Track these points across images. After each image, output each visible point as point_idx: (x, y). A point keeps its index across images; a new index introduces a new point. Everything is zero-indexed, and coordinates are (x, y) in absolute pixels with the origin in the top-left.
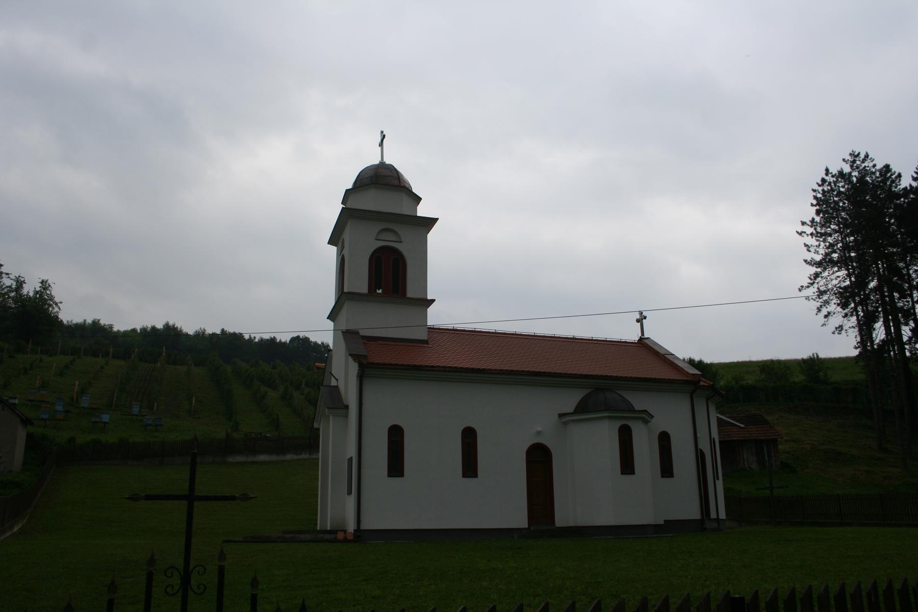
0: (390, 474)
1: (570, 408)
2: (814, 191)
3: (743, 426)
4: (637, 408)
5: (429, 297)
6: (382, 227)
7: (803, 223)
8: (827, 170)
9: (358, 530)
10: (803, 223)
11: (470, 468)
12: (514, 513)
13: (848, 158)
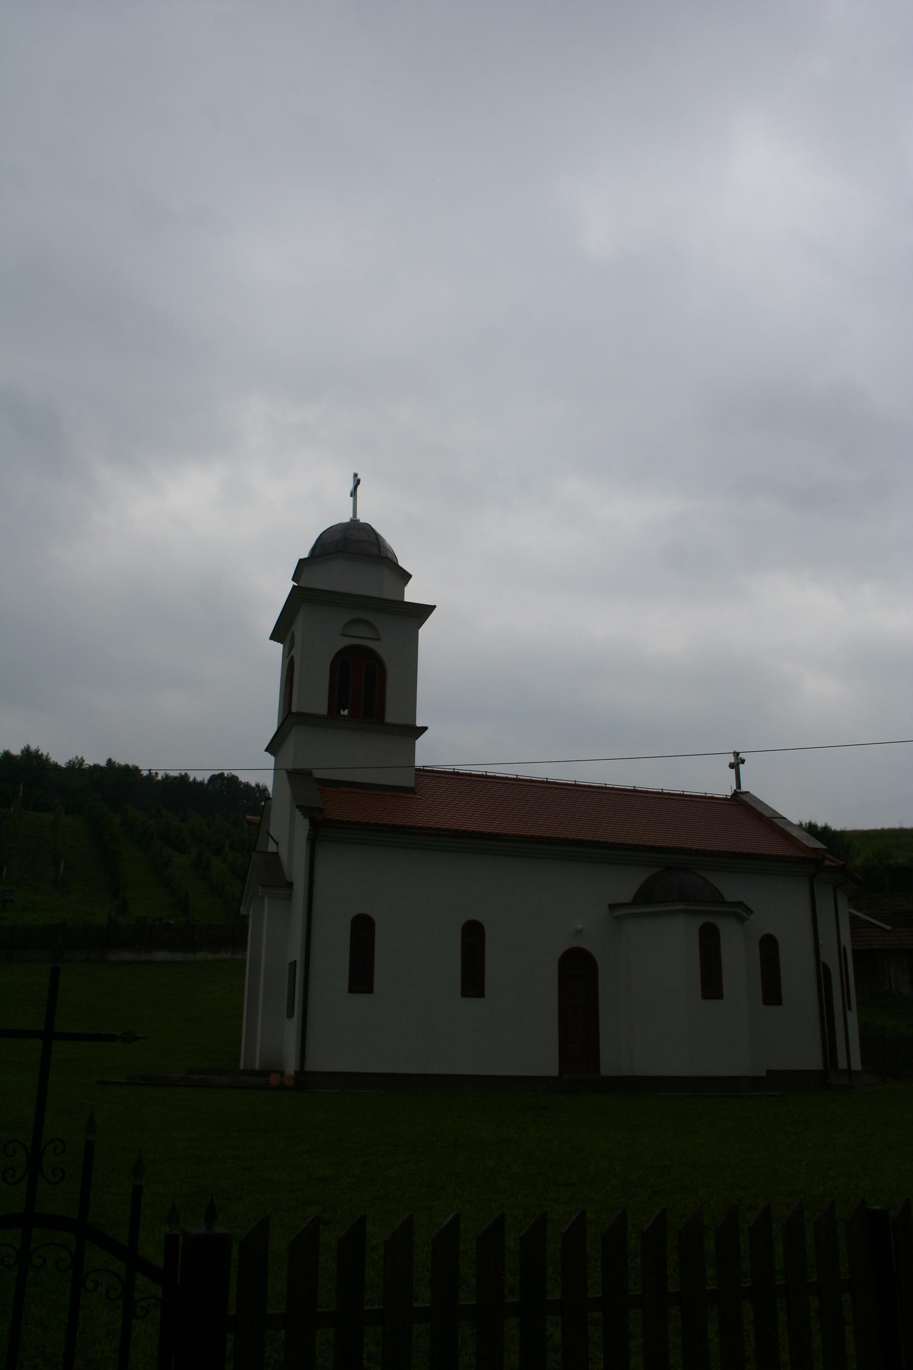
3: (888, 928)
4: (728, 898)
5: (419, 723)
6: (350, 615)
11: (473, 982)
12: (541, 1057)
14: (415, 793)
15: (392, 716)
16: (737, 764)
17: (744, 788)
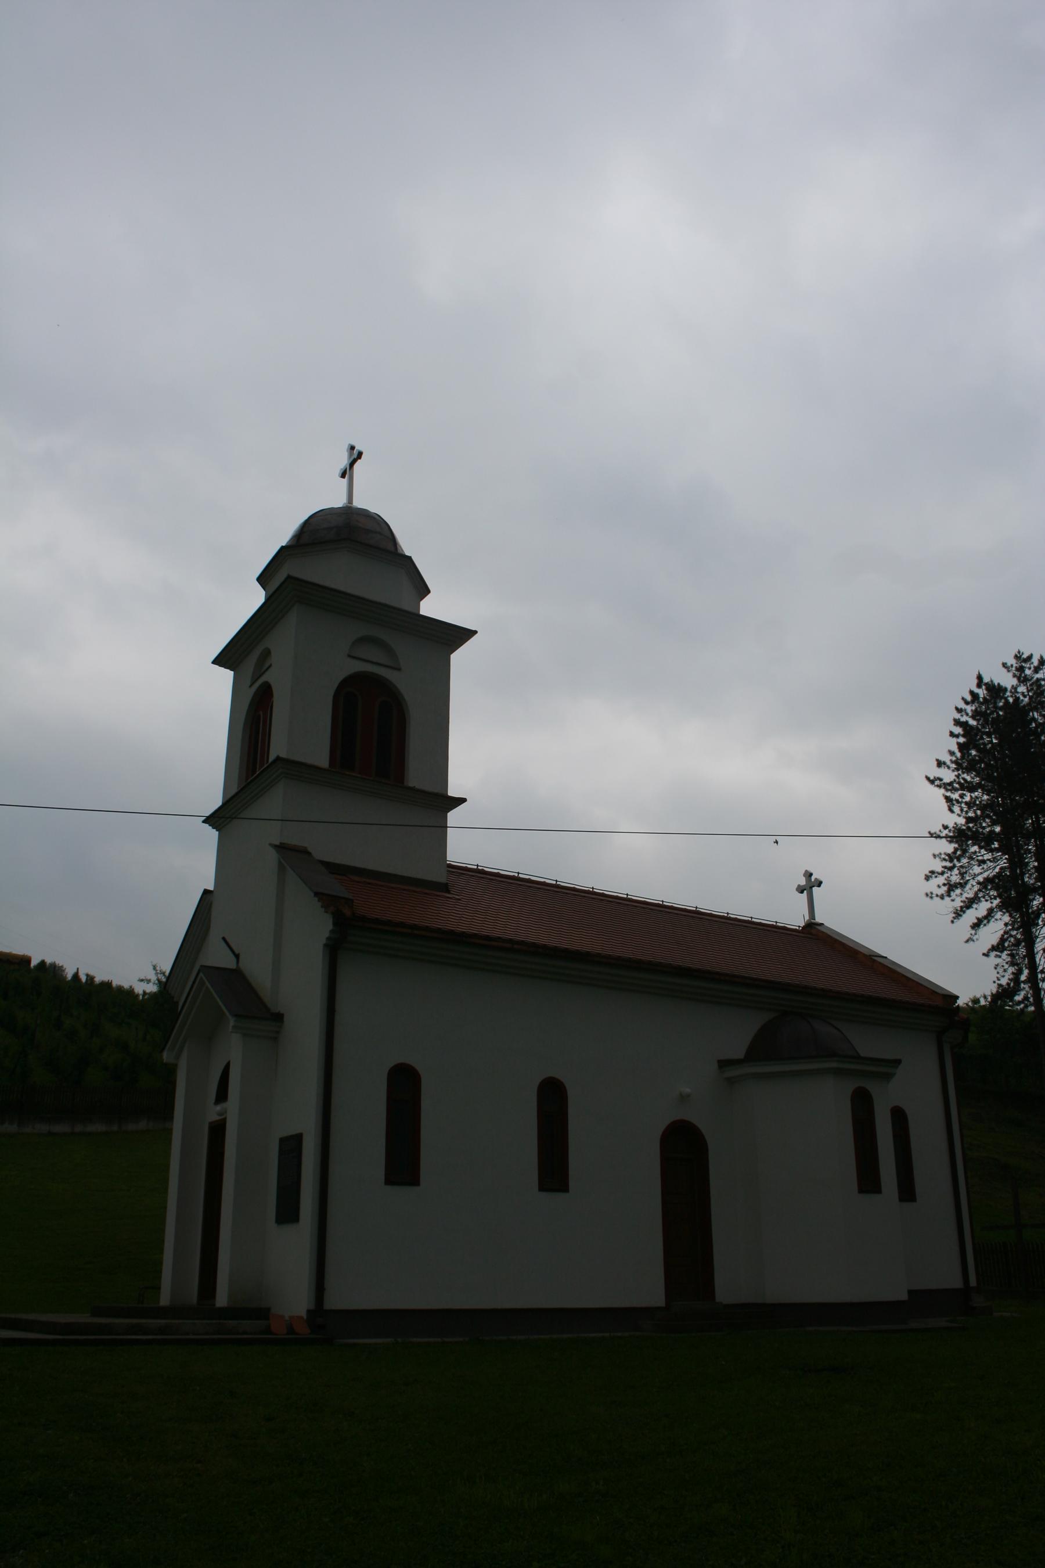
0: (391, 1179)
1: (738, 1052)
2: (959, 710)
5: (452, 792)
7: (940, 764)
8: (980, 678)
9: (318, 1313)
10: (940, 764)
11: (554, 1173)
12: (638, 1280)
13: (1012, 661)
14: (448, 892)
15: (416, 777)
16: (810, 885)
17: (819, 919)
